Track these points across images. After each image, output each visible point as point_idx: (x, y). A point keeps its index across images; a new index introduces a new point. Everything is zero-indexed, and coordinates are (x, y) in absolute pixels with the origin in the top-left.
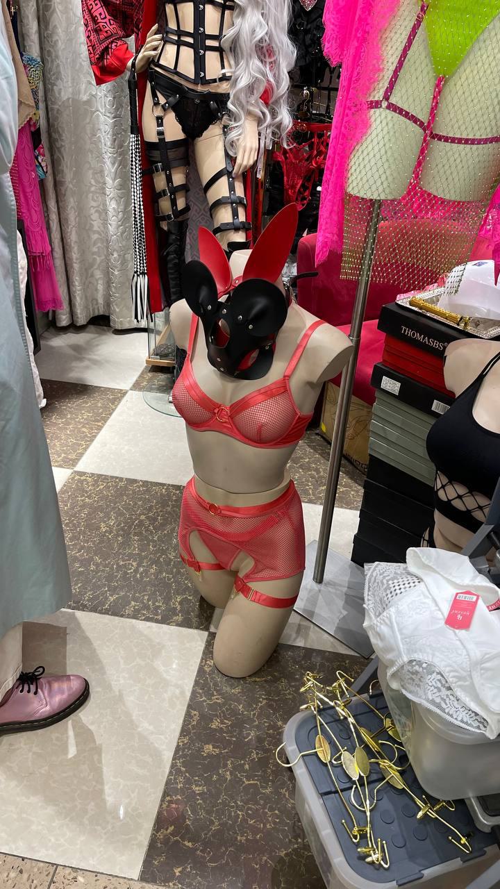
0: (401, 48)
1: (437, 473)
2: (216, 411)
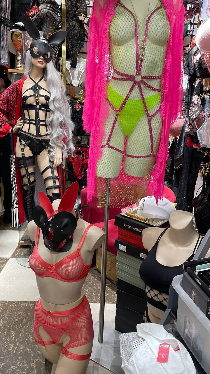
0: (111, 128)
1: (145, 285)
2: (49, 268)
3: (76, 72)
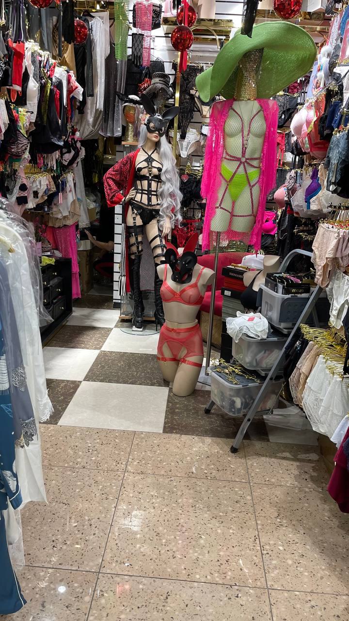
3: (185, 143)
